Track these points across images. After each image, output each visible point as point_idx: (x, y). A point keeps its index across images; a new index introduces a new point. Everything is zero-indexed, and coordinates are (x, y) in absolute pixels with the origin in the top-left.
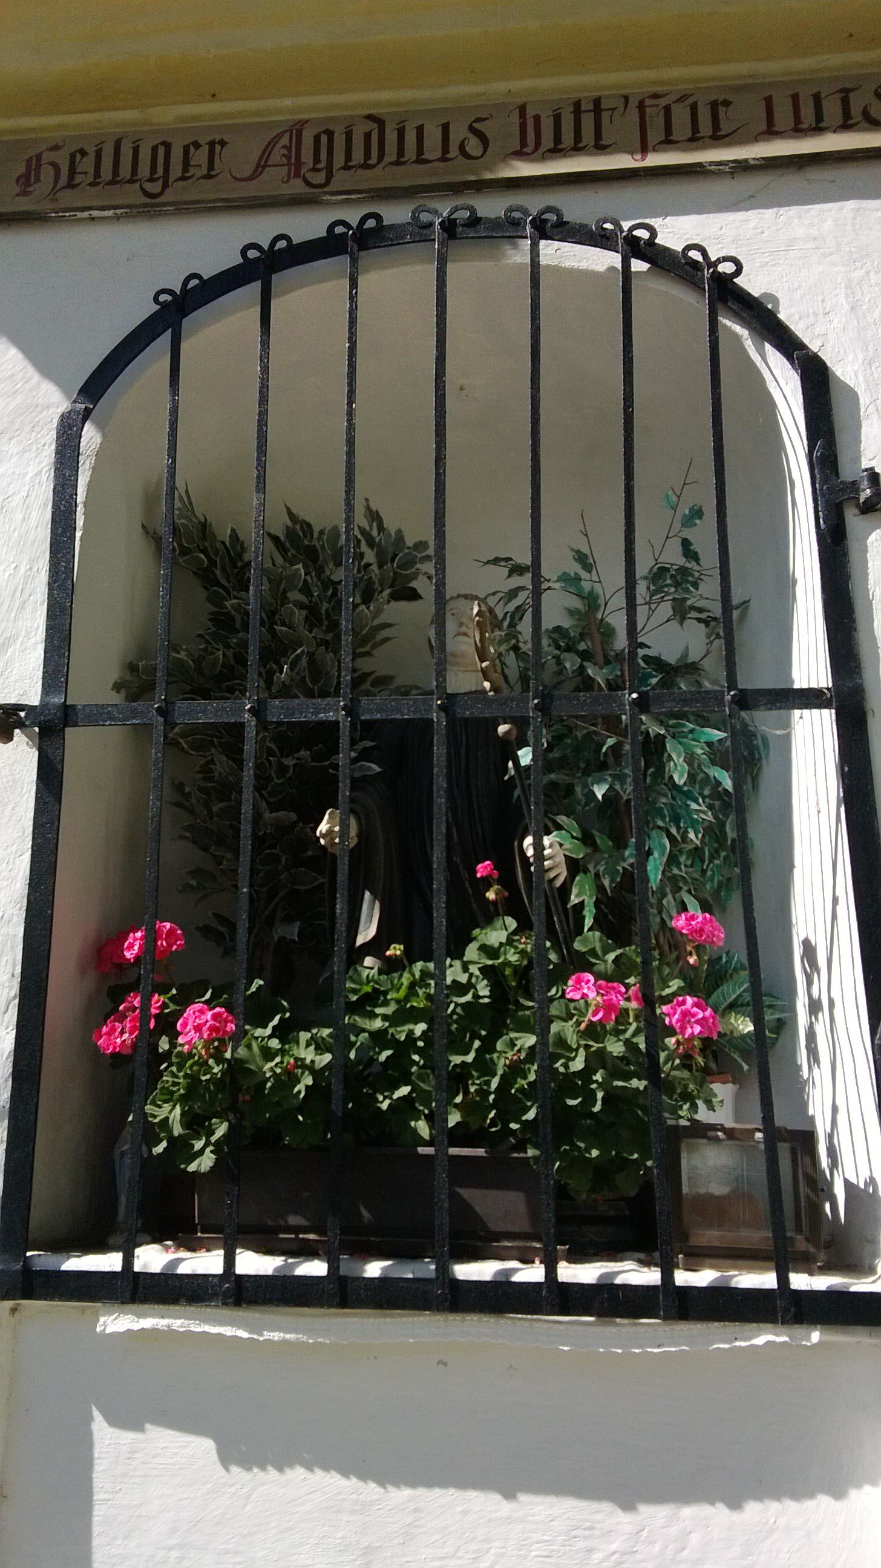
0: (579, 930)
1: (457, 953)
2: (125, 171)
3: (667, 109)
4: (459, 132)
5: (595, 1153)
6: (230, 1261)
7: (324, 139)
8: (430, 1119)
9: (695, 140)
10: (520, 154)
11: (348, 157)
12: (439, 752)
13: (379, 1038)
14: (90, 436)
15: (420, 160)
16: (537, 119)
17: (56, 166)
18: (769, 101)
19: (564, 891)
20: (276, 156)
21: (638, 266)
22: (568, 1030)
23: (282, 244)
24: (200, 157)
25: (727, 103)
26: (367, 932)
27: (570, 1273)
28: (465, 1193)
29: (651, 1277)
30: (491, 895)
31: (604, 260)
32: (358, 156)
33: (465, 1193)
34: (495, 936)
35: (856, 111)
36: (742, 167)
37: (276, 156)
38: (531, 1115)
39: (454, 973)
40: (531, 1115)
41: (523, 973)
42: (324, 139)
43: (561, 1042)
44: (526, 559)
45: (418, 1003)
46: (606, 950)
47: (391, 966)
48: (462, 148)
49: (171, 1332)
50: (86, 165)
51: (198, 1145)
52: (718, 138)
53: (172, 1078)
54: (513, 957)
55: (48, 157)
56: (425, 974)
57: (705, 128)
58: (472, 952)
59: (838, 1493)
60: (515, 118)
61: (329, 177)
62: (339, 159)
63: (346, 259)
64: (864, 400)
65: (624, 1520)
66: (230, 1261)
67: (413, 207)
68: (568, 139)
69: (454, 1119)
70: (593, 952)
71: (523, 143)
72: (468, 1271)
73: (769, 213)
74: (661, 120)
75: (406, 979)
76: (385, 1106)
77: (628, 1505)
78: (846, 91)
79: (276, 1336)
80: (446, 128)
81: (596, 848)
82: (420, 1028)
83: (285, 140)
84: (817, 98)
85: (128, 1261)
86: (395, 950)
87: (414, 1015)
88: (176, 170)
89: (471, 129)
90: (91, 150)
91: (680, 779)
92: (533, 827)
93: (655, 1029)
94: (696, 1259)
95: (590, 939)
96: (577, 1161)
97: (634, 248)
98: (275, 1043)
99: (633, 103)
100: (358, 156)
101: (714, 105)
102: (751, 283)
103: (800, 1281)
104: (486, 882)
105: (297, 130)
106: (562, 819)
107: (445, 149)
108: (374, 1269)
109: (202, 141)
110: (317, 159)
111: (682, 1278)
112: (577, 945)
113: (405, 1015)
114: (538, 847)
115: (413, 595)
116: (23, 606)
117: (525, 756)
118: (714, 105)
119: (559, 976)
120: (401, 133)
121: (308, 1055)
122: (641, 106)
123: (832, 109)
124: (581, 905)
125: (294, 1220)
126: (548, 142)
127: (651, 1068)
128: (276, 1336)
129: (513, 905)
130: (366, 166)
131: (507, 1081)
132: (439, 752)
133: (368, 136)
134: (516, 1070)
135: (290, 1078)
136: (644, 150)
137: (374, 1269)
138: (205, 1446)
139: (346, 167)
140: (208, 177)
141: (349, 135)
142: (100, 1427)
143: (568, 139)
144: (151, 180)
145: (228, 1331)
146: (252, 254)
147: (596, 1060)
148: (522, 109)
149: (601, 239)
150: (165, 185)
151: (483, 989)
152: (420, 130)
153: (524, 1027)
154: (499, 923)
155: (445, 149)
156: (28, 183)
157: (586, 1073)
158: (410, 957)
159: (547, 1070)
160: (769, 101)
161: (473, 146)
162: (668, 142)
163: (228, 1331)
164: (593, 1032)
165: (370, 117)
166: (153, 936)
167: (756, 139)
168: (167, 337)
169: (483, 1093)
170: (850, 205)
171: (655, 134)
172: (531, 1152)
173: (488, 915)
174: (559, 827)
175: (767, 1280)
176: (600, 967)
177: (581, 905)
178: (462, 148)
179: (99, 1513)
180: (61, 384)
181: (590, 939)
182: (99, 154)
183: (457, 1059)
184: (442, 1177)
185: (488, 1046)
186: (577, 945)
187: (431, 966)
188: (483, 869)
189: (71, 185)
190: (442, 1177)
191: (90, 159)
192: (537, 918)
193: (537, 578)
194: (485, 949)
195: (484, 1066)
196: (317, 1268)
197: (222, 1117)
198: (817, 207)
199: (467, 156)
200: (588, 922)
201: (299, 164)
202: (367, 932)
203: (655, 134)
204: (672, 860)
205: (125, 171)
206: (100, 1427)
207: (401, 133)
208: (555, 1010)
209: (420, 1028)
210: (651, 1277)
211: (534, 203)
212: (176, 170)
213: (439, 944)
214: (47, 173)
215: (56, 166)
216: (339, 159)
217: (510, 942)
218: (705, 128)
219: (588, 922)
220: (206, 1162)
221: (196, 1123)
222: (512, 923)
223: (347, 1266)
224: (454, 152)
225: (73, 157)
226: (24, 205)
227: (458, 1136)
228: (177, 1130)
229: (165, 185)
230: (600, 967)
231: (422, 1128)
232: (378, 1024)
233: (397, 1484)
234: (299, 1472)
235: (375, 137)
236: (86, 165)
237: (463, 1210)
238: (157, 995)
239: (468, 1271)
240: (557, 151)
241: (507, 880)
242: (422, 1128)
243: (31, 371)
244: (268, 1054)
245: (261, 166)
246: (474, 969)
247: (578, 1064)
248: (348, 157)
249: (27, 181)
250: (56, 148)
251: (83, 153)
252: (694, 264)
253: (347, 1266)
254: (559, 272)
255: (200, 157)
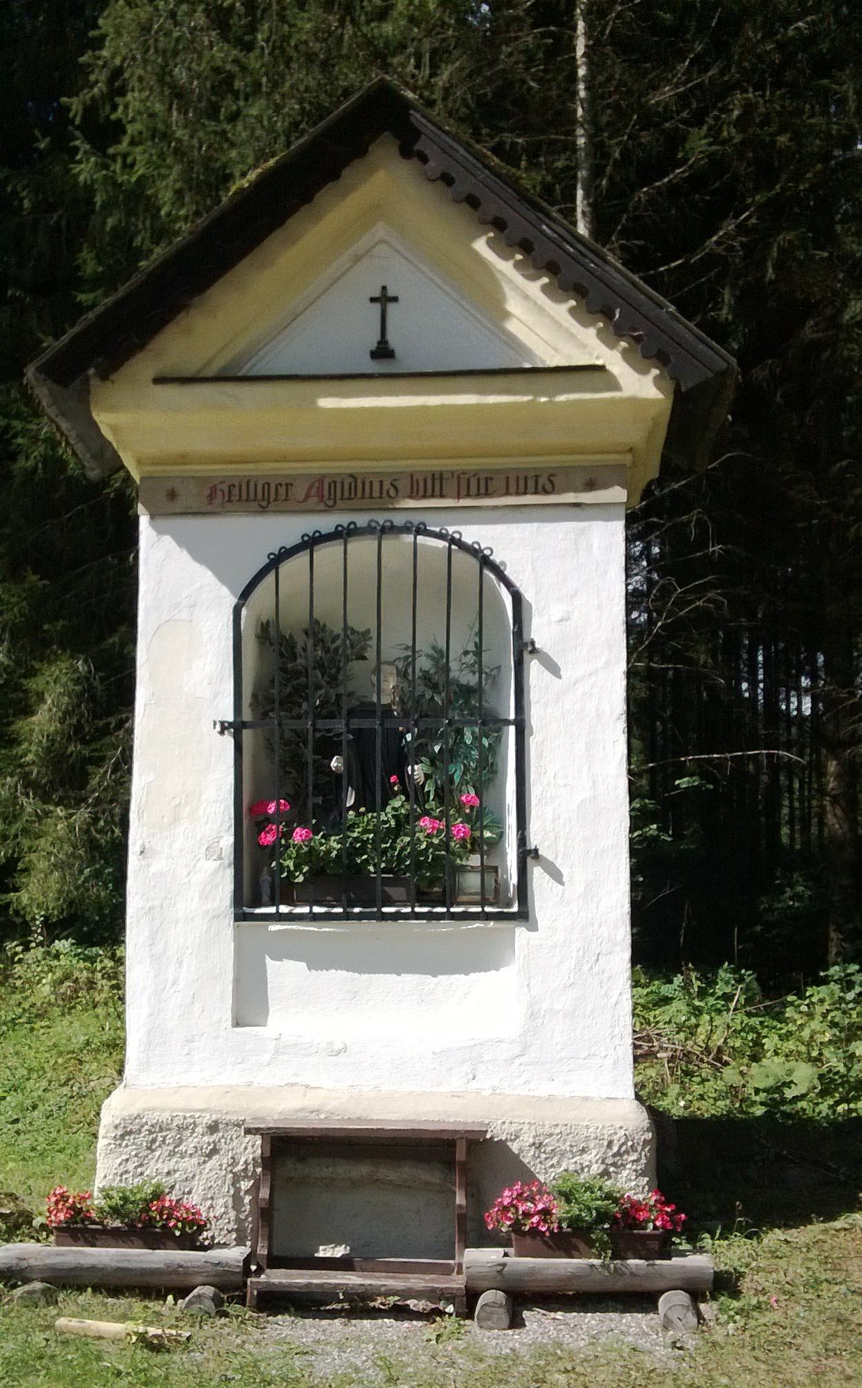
0: (428, 801)
1: (383, 809)
2: (252, 496)
3: (468, 480)
4: (386, 486)
5: (428, 874)
6: (311, 909)
7: (333, 485)
8: (375, 865)
9: (478, 495)
10: (411, 497)
11: (342, 494)
12: (379, 741)
13: (356, 839)
14: (244, 612)
15: (371, 497)
16: (418, 481)
17: (223, 491)
18: (508, 478)
19: (423, 786)
20: (313, 492)
21: (453, 547)
22: (421, 835)
23: (317, 534)
24: (282, 490)
25: (491, 479)
26: (350, 802)
27: (417, 910)
28: (386, 889)
29: (444, 910)
30: (396, 788)
31: (442, 544)
32: (346, 495)
33: (386, 889)
34: (397, 803)
35: (540, 488)
36: (495, 508)
37: (313, 492)
38: (408, 863)
39: (383, 817)
40: (408, 863)
41: (407, 816)
42: (333, 485)
43: (418, 839)
44: (410, 644)
45: (370, 827)
46: (437, 808)
47: (359, 814)
48: (388, 492)
49: (292, 930)
50: (235, 492)
51: (297, 874)
52: (487, 494)
53: (292, 851)
54: (403, 811)
55: (219, 487)
56: (372, 817)
57: (483, 490)
58: (388, 809)
59: (497, 969)
60: (409, 481)
61: (335, 502)
62: (339, 495)
63: (342, 540)
64: (534, 607)
65: (434, 980)
66: (311, 909)
67: (370, 518)
68: (429, 492)
69: (383, 865)
70: (432, 809)
71: (412, 492)
72: (385, 910)
73: (505, 526)
74: (466, 484)
75: (366, 819)
76: (359, 861)
77: (435, 976)
78: (537, 476)
79: (327, 930)
80: (381, 482)
81: (437, 768)
82: (371, 836)
83: (317, 485)
84: (526, 479)
85: (277, 909)
86: (362, 809)
87: (369, 832)
88: (273, 496)
89: (392, 484)
90: (237, 484)
91: (468, 742)
92: (410, 759)
93: (449, 837)
94: (459, 904)
95: (431, 804)
96: (423, 878)
97: (453, 541)
98: (323, 841)
99: (455, 476)
100: (346, 495)
101: (487, 479)
102: (496, 558)
103: (488, 909)
104: (395, 784)
105: (321, 479)
106: (423, 759)
107: (381, 493)
108: (357, 910)
109: (284, 483)
110: (330, 495)
111: (452, 910)
112: (427, 807)
113: (365, 831)
114: (413, 770)
115: (364, 658)
116: (222, 680)
117: (409, 737)
118: (487, 479)
119: (418, 818)
120: (364, 484)
121: (335, 845)
122: (459, 478)
123: (531, 484)
124: (429, 792)
125: (328, 898)
126: (421, 493)
127: (447, 848)
128: (327, 930)
129: (404, 791)
130: (350, 499)
131: (400, 853)
132: (379, 741)
133: (350, 484)
134: (403, 849)
135: (329, 852)
136: (459, 497)
137: (357, 910)
138: (304, 964)
139: (342, 499)
140: (286, 500)
141: (342, 484)
142: (268, 960)
143: (429, 492)
144: (263, 500)
145: (312, 929)
146: (306, 538)
147: (430, 845)
148: (412, 476)
149: (440, 536)
150: (269, 503)
151: (393, 823)
152: (371, 482)
153: (406, 835)
154: (398, 798)
155: (381, 493)
156: (211, 500)
157: (426, 849)
158: (368, 811)
159: (414, 849)
160: (508, 478)
161: (392, 493)
162: (468, 495)
163: (312, 929)
164: (429, 836)
165: (351, 476)
166: (279, 804)
167: (502, 495)
168: (273, 572)
169: (392, 856)
170: (536, 525)
171: (463, 492)
172: (408, 875)
173: (395, 795)
174: (422, 762)
175: (479, 909)
176: (434, 814)
177: (429, 792)
178: (388, 492)
179: (269, 986)
180: (232, 590)
181: (431, 804)
182: (240, 486)
183: (383, 846)
184: (379, 882)
185: (394, 841)
186: (427, 807)
187: (375, 814)
188: (393, 779)
189: (229, 501)
190: (379, 882)
191: (237, 488)
192: (412, 794)
193: (414, 651)
194: (393, 809)
195: (393, 848)
196: (340, 910)
197: (306, 864)
198: (523, 525)
199: (390, 497)
200: (432, 797)
201: (323, 496)
202: (350, 802)
203: (463, 492)
204: (464, 773)
205: (252, 496)
206: (268, 960)
207: (364, 484)
208: (417, 829)
209: (371, 836)
210: (444, 910)
211: (416, 519)
212: (273, 496)
213: (378, 807)
214: (219, 493)
215: (223, 491)
216: (339, 495)
217: (402, 806)
218: (483, 490)
219: (432, 797)
220: (301, 879)
221: (298, 867)
222: (403, 798)
223: (348, 910)
224: (385, 494)
225: (229, 487)
226: (210, 509)
227: (384, 871)
228: (292, 868)
229: (269, 503)
230: (434, 814)
231: (371, 868)
232: (355, 835)
233: (364, 973)
234: (333, 971)
235: (353, 484)
236: (235, 492)
237: (385, 893)
238: (726, 964)
239: (385, 910)
240: (425, 497)
241: (402, 782)
242: (371, 868)
243: (217, 582)
244: (322, 844)
245: (307, 496)
246: (390, 816)
247: (424, 846)
248: (342, 494)
249: (211, 497)
250: (222, 482)
251: (234, 486)
252: (475, 549)
253: (349, 910)
254: (424, 546)
255: (282, 490)
